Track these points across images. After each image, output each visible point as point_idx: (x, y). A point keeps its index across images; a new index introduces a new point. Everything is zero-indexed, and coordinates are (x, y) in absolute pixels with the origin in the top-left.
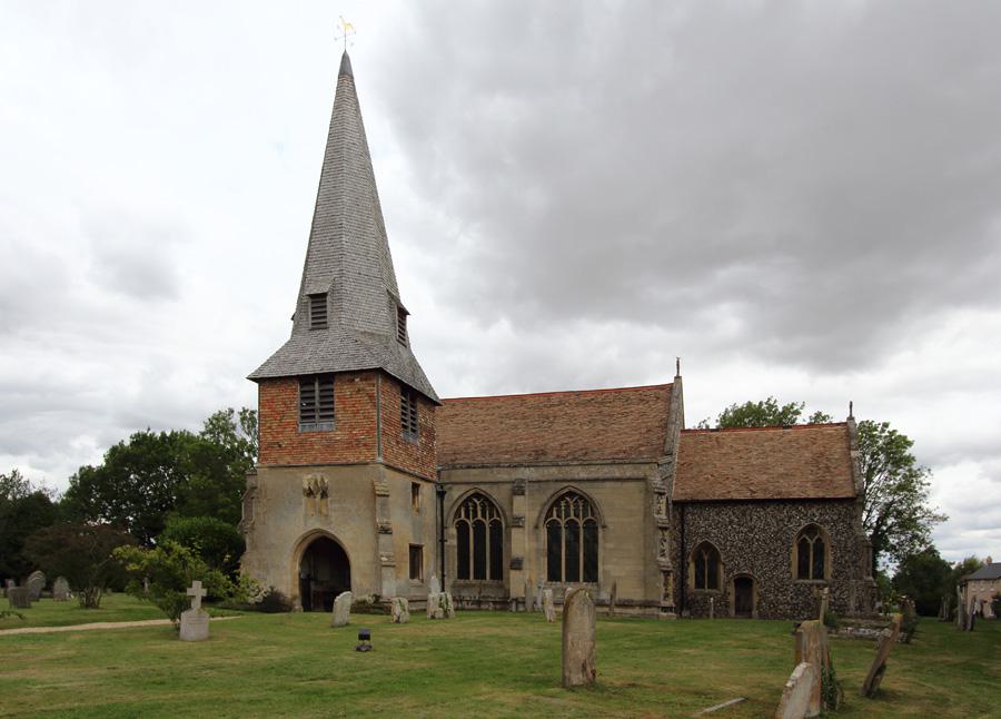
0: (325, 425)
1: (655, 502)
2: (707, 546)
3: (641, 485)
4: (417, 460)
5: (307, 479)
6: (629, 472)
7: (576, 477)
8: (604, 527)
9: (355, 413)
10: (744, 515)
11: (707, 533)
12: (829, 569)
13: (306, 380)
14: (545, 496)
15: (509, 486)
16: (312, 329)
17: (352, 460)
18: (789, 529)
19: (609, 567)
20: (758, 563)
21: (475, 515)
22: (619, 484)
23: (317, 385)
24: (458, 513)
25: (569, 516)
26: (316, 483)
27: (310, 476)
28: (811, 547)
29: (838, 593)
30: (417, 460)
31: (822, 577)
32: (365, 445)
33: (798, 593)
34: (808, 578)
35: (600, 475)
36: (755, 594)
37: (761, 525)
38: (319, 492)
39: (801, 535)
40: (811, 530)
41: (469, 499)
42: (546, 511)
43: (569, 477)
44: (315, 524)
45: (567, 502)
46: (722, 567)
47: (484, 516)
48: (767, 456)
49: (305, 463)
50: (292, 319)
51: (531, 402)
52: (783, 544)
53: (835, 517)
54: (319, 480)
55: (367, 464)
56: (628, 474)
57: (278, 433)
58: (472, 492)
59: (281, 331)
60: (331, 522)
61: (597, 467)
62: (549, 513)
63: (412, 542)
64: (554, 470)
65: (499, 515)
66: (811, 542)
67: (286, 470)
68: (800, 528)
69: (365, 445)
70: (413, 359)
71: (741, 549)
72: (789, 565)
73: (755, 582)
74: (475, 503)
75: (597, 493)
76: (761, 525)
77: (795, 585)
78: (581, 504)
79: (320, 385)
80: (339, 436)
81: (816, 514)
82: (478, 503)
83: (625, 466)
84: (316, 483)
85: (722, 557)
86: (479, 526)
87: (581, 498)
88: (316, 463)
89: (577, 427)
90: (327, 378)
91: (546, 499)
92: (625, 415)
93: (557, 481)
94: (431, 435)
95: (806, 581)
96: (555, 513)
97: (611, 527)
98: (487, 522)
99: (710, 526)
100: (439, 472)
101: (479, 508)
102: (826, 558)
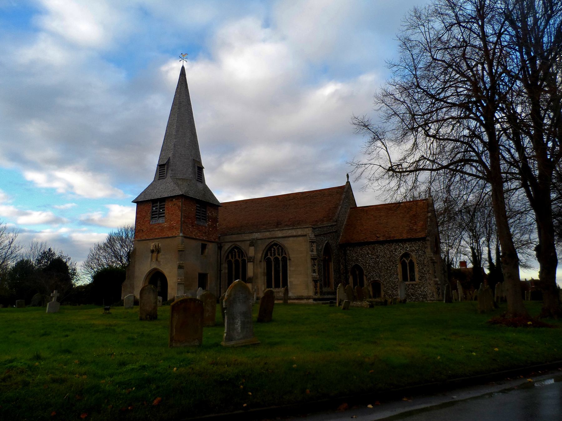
2: (357, 267)
4: (205, 233)
5: (152, 245)
7: (277, 236)
9: (173, 214)
10: (374, 249)
11: (357, 260)
12: (417, 276)
14: (262, 247)
15: (249, 242)
16: (159, 179)
17: (170, 236)
18: (396, 255)
20: (382, 274)
21: (235, 257)
22: (295, 238)
23: (158, 203)
24: (228, 257)
26: (156, 246)
27: (154, 244)
28: (408, 265)
29: (422, 288)
30: (205, 233)
31: (414, 280)
32: (176, 228)
34: (407, 281)
35: (287, 235)
38: (157, 251)
40: (406, 255)
44: (154, 266)
45: (274, 248)
46: (365, 277)
47: (239, 257)
49: (152, 238)
52: (394, 263)
54: (157, 245)
55: (176, 237)
56: (299, 233)
57: (142, 225)
58: (233, 246)
59: (150, 178)
61: (286, 231)
62: (266, 255)
63: (201, 272)
64: (268, 233)
65: (285, 254)
66: (407, 262)
67: (144, 242)
68: (401, 255)
69: (176, 228)
70: (206, 187)
71: (374, 267)
72: (397, 274)
73: (381, 284)
74: (235, 251)
75: (288, 244)
79: (160, 203)
80: (166, 225)
82: (236, 251)
83: (298, 230)
84: (156, 246)
85: (365, 272)
86: (237, 261)
87: (280, 246)
88: (156, 237)
90: (163, 200)
91: (264, 248)
93: (269, 238)
94: (215, 220)
96: (269, 254)
97: (292, 259)
98: (240, 260)
99: (358, 256)
100: (219, 237)
101: (237, 254)
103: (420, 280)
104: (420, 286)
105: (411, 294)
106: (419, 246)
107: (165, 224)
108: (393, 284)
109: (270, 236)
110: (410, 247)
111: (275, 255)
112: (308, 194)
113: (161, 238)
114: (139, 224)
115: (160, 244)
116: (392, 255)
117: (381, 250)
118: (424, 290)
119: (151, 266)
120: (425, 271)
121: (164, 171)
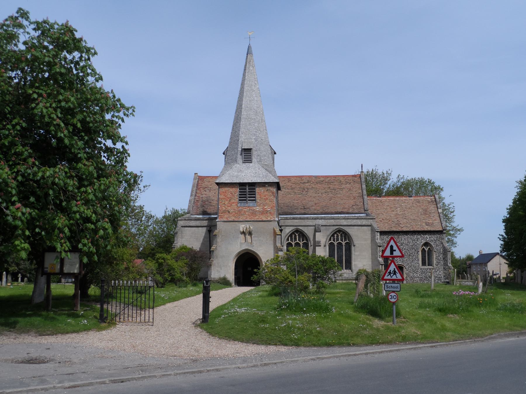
0: (251, 204)
1: (376, 235)
3: (370, 228)
5: (242, 227)
6: (364, 222)
8: (354, 246)
13: (242, 185)
19: (356, 263)
22: (360, 227)
23: (247, 186)
24: (288, 240)
25: (338, 240)
26: (246, 229)
29: (438, 272)
32: (270, 213)
33: (422, 272)
36: (404, 273)
37: (406, 242)
39: (422, 246)
40: (426, 244)
41: (293, 233)
42: (329, 238)
43: (338, 224)
44: (244, 247)
48: (404, 211)
49: (242, 220)
50: (224, 154)
51: (293, 180)
53: (435, 239)
54: (248, 227)
60: (253, 246)
62: (330, 240)
66: (427, 250)
67: (232, 223)
68: (422, 244)
72: (418, 260)
73: (404, 268)
75: (351, 231)
76: (406, 242)
77: (421, 269)
78: (343, 235)
80: (258, 209)
81: (428, 238)
87: (344, 233)
89: (320, 195)
90: (253, 185)
92: (342, 189)
93: (334, 226)
95: (425, 267)
97: (357, 245)
102: (432, 257)
103: (437, 265)
104: (436, 270)
105: (429, 276)
106: (437, 237)
107: (257, 207)
108: (414, 268)
109: (335, 224)
110: (430, 237)
111: (338, 240)
112: (322, 179)
113: (253, 221)
114: (223, 205)
115: (251, 227)
116: (415, 244)
117: (405, 239)
118: (440, 273)
119: (241, 247)
120: (441, 258)
121: (244, 156)
